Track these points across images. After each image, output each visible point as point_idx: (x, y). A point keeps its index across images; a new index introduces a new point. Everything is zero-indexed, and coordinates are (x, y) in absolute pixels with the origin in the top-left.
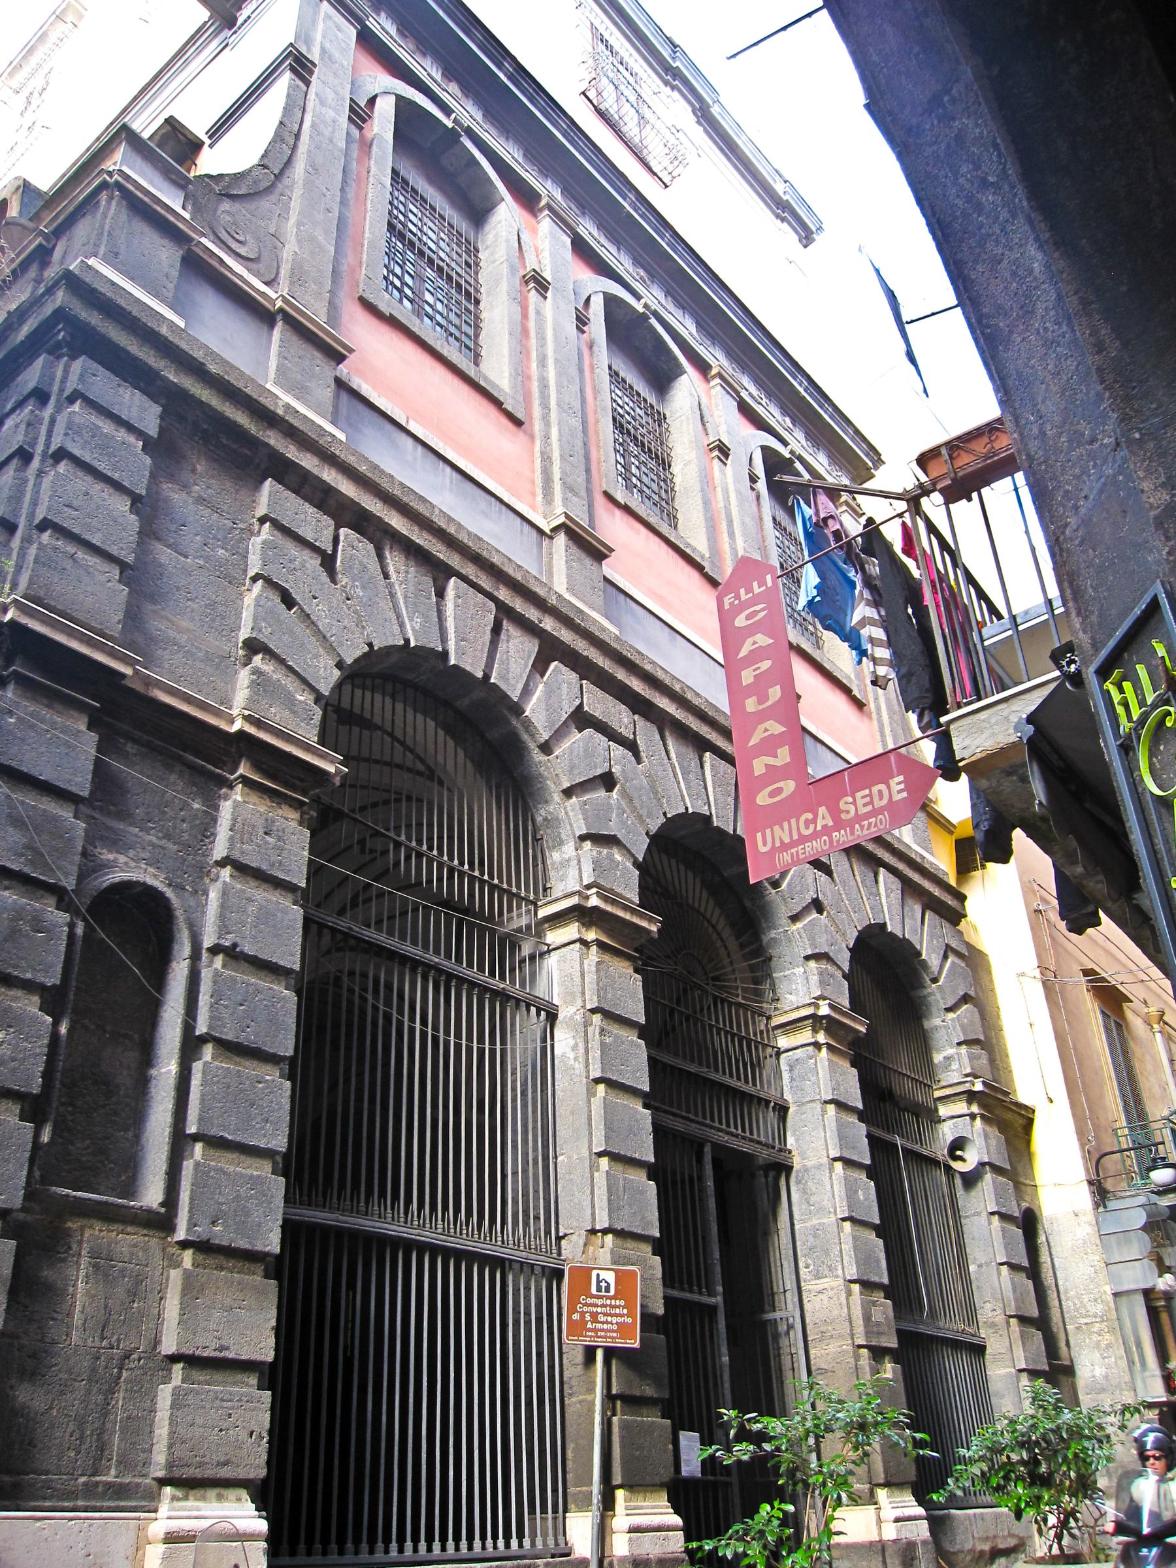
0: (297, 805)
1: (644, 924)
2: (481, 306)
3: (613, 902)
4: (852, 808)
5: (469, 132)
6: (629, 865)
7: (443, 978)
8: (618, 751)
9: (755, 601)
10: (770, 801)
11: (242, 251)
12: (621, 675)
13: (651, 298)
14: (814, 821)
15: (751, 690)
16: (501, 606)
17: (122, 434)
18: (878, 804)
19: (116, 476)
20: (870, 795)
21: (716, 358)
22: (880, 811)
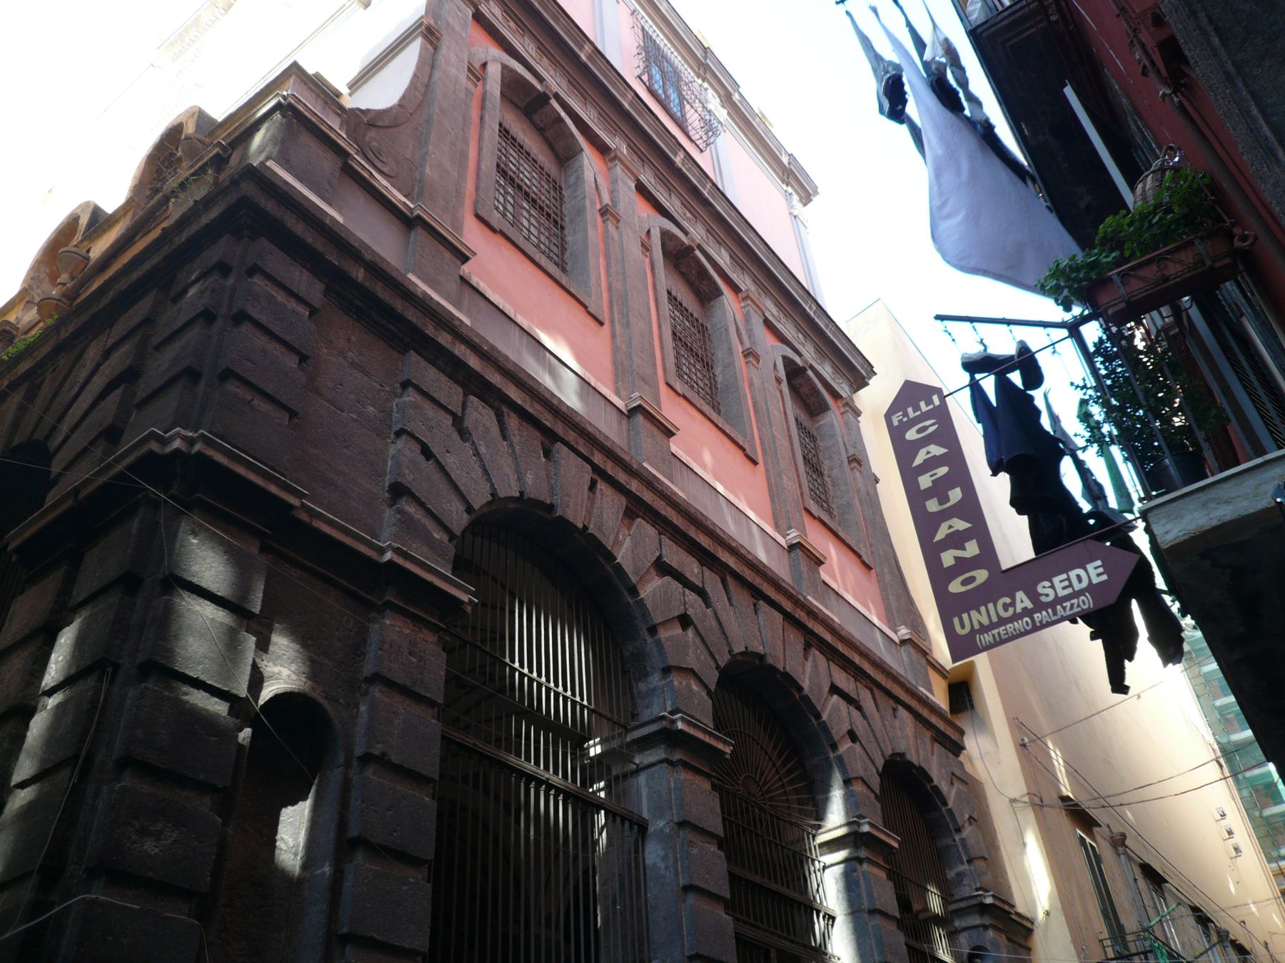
0: (435, 629)
1: (720, 746)
2: (566, 232)
3: (695, 726)
4: (1050, 591)
5: (557, 96)
6: (704, 694)
7: (552, 792)
8: (691, 597)
9: (926, 416)
10: (963, 589)
11: (385, 169)
12: (693, 532)
13: (697, 233)
14: (1013, 604)
15: (929, 493)
16: (597, 470)
17: (293, 304)
18: (1077, 586)
19: (287, 338)
20: (1069, 579)
21: (745, 282)
22: (1081, 593)
